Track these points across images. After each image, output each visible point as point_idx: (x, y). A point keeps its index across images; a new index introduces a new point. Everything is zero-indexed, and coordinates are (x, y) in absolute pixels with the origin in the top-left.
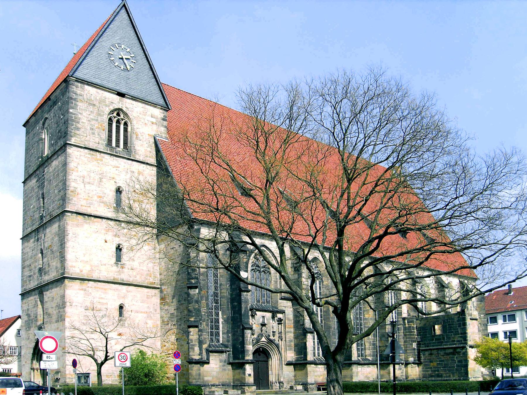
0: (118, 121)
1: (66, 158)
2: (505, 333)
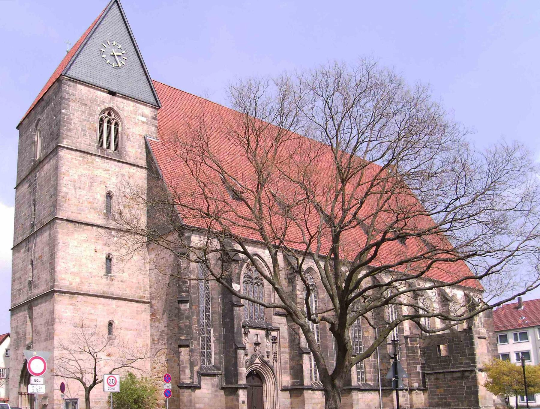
0: (109, 121)
1: (57, 161)
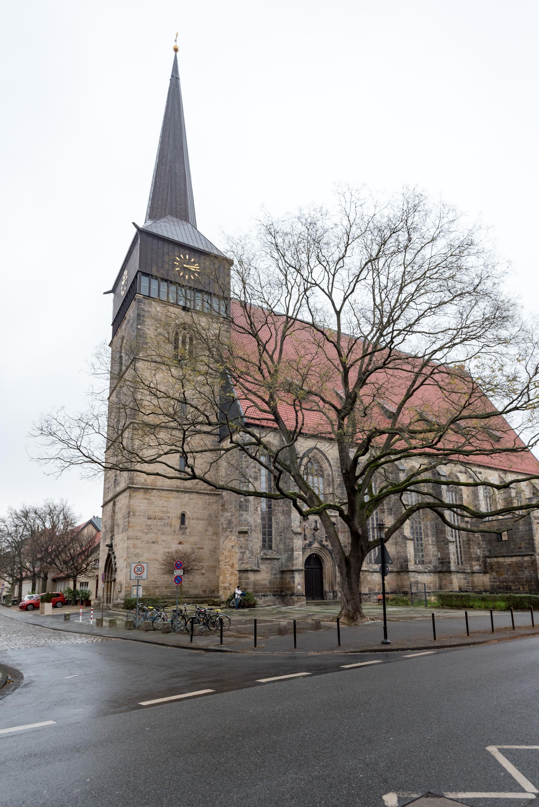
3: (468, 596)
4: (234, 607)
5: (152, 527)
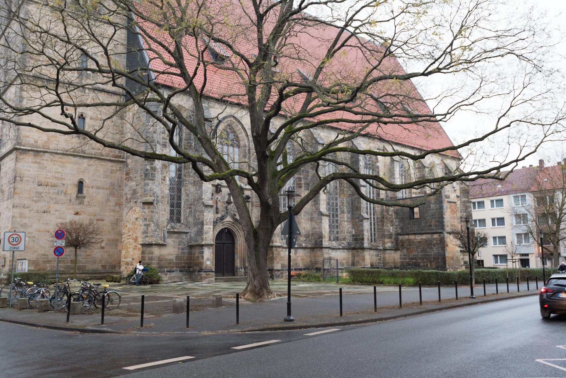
2: (493, 220)
3: (379, 272)
4: (135, 284)
5: (43, 195)
